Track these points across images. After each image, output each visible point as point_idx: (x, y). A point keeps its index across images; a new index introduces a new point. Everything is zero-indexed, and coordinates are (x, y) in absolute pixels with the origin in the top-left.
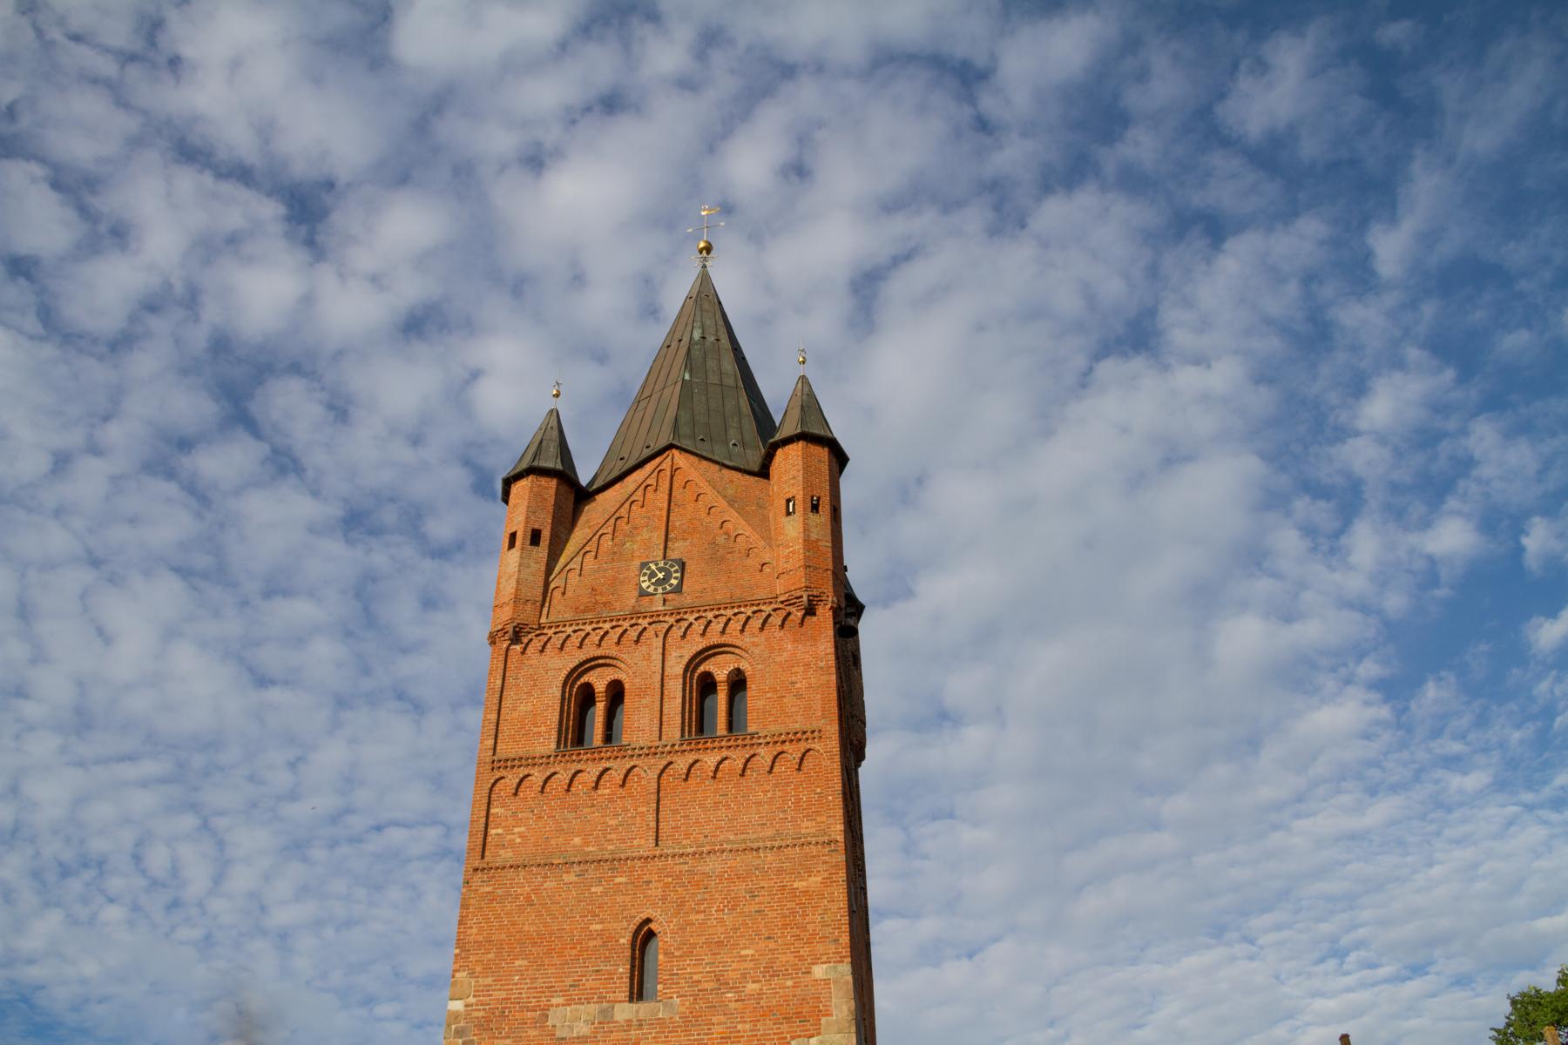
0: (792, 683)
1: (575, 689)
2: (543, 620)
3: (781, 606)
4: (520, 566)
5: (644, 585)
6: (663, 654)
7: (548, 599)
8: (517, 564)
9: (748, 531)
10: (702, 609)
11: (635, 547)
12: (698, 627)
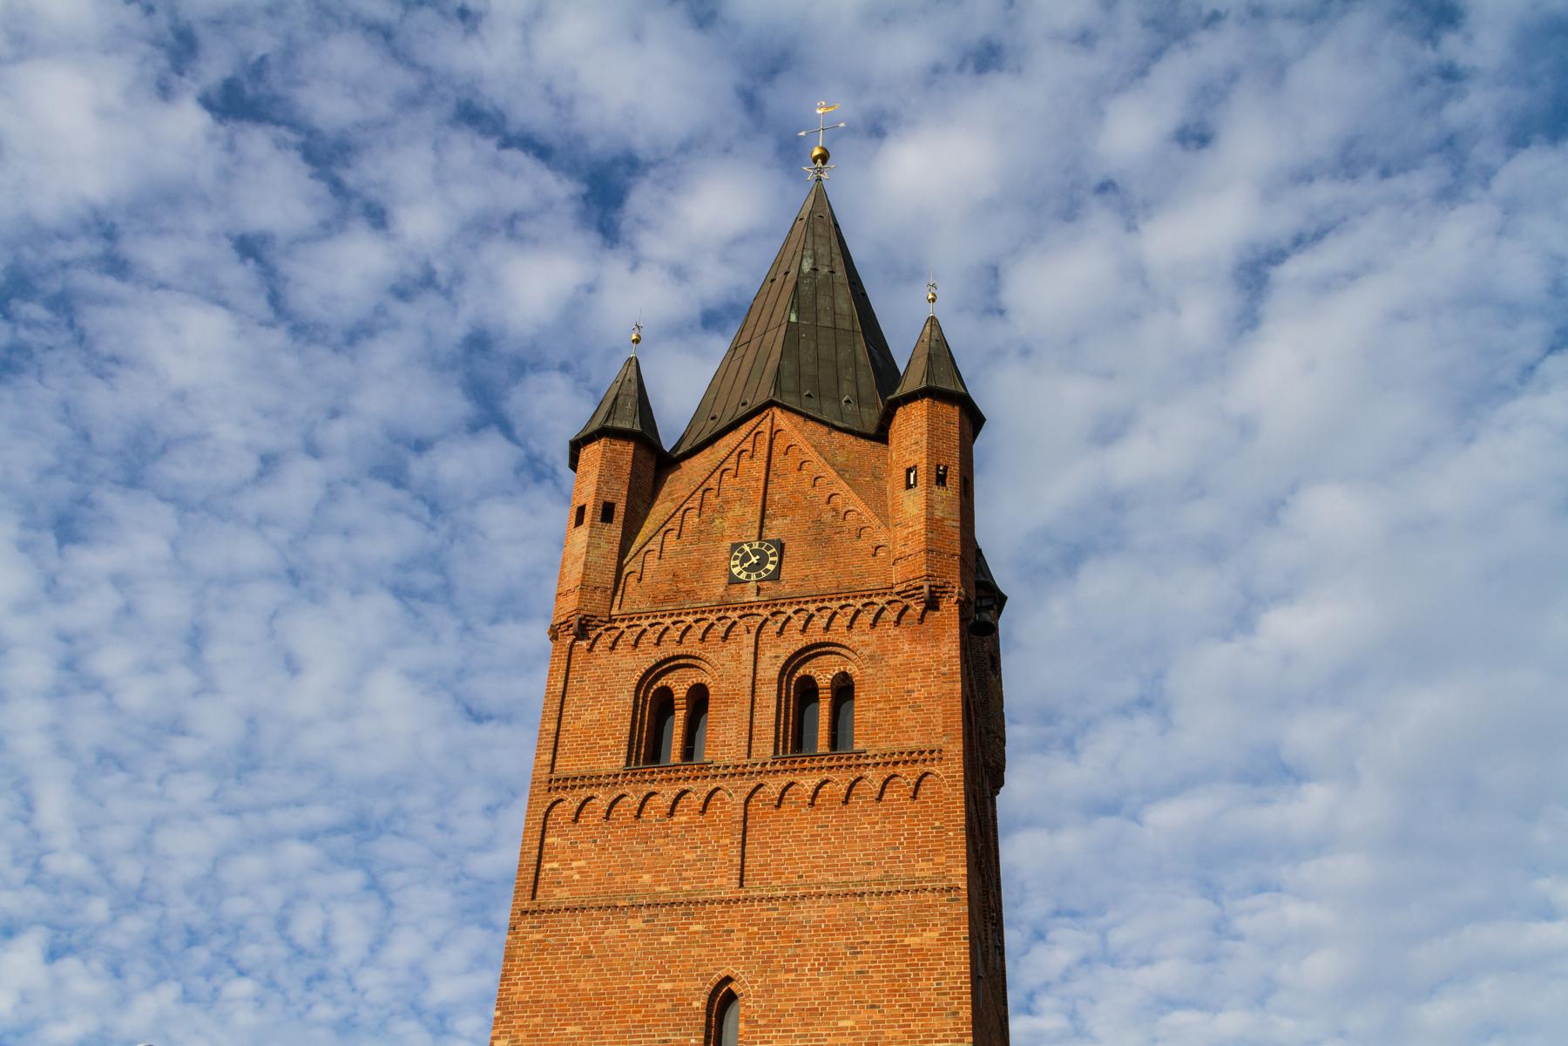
0: (908, 691)
1: (650, 695)
2: (615, 611)
3: (897, 598)
5: (735, 571)
6: (756, 654)
8: (585, 544)
11: (726, 524)
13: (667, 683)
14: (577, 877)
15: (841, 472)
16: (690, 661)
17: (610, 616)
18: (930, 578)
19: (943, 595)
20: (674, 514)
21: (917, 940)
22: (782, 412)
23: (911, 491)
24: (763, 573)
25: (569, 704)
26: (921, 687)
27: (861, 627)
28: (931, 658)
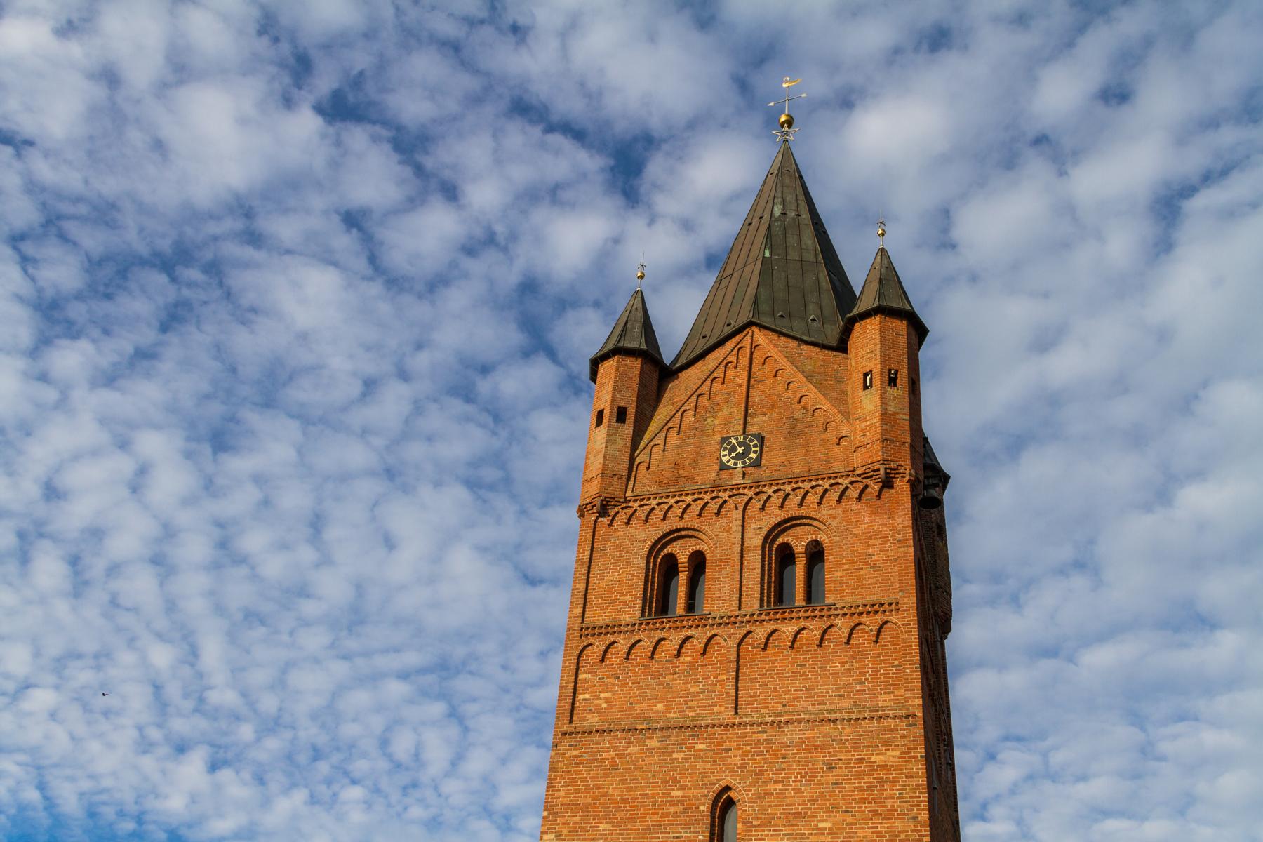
0: (870, 555)
2: (629, 494)
3: (858, 479)
4: (607, 442)
5: (725, 459)
6: (743, 526)
7: (634, 473)
9: (826, 405)
10: (780, 482)
12: (776, 500)
13: (672, 550)
14: (604, 705)
15: (809, 378)
16: (690, 533)
17: (626, 498)
18: (886, 462)
19: (897, 476)
20: (674, 415)
21: (882, 758)
22: (759, 330)
23: (868, 391)
24: (747, 461)
25: (594, 568)
26: (880, 551)
27: (829, 503)
28: (888, 527)
